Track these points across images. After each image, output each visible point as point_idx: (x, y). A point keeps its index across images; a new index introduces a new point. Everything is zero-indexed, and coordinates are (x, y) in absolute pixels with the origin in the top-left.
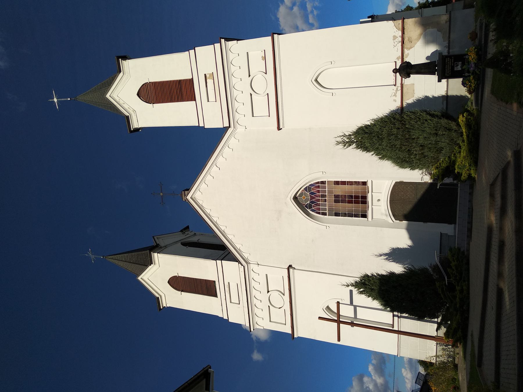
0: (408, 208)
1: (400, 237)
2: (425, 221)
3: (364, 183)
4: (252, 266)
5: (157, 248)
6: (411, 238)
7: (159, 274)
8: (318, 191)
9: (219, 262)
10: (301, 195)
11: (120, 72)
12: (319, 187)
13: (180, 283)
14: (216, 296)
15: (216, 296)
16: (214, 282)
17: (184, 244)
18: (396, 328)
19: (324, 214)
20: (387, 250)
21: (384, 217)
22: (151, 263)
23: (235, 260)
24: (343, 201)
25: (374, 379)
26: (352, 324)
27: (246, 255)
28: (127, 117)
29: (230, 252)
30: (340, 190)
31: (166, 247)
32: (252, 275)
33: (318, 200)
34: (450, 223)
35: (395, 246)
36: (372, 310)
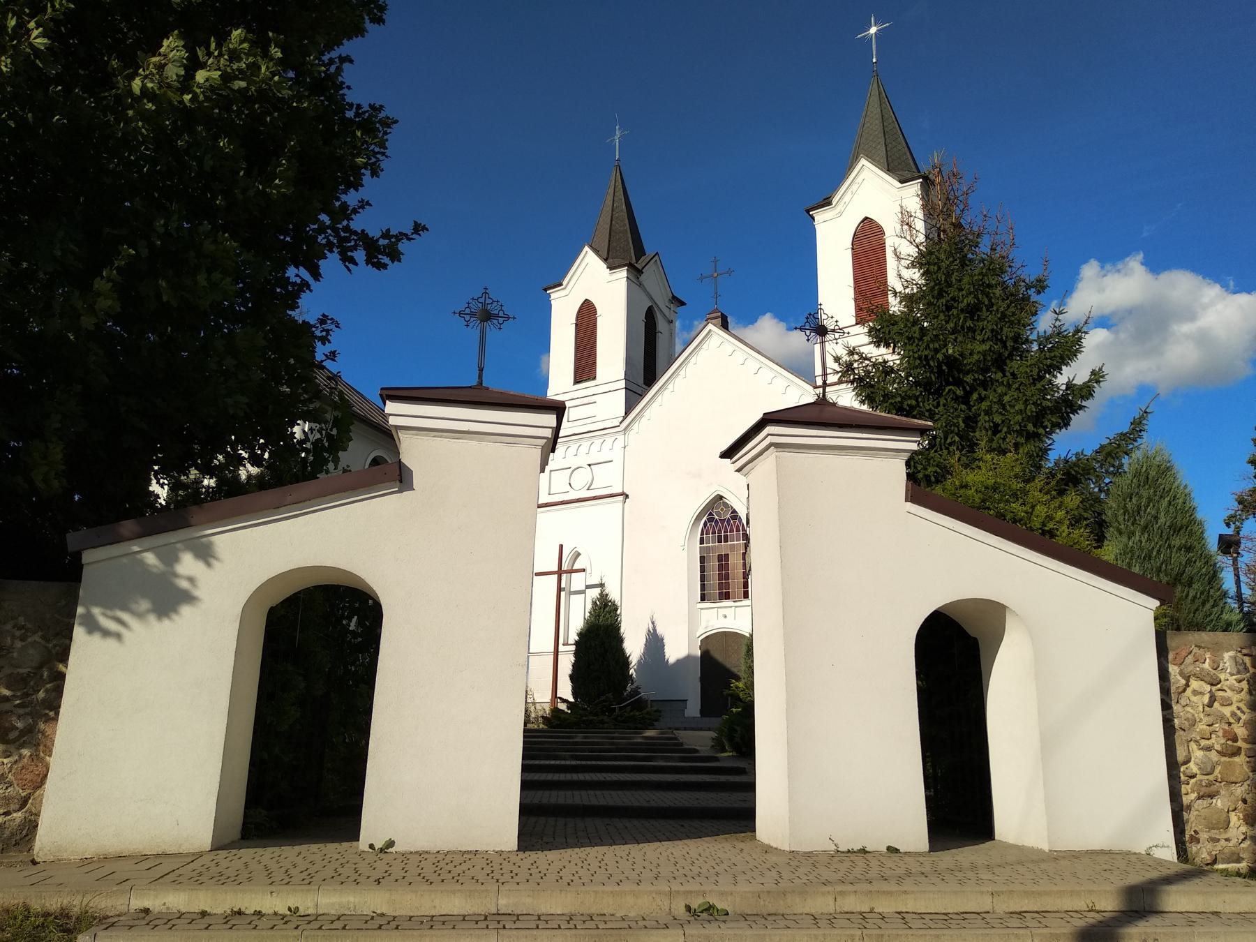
0: (718, 655)
1: (678, 648)
2: (702, 679)
3: (746, 595)
4: (621, 438)
5: (636, 273)
6: (678, 661)
7: (595, 283)
8: (732, 531)
9: (623, 384)
10: (726, 505)
11: (902, 182)
12: (738, 530)
13: (587, 316)
14: (577, 382)
15: (577, 382)
16: (594, 378)
17: (650, 316)
18: (561, 648)
19: (702, 542)
20: (660, 631)
21: (704, 624)
22: (611, 268)
23: (627, 413)
24: (720, 568)
25: (26, 652)
26: (560, 590)
27: (635, 427)
28: (830, 203)
29: (642, 396)
30: (735, 560)
31: (640, 285)
32: (609, 440)
33: (720, 531)
34: (702, 712)
35: (665, 641)
36: (577, 617)
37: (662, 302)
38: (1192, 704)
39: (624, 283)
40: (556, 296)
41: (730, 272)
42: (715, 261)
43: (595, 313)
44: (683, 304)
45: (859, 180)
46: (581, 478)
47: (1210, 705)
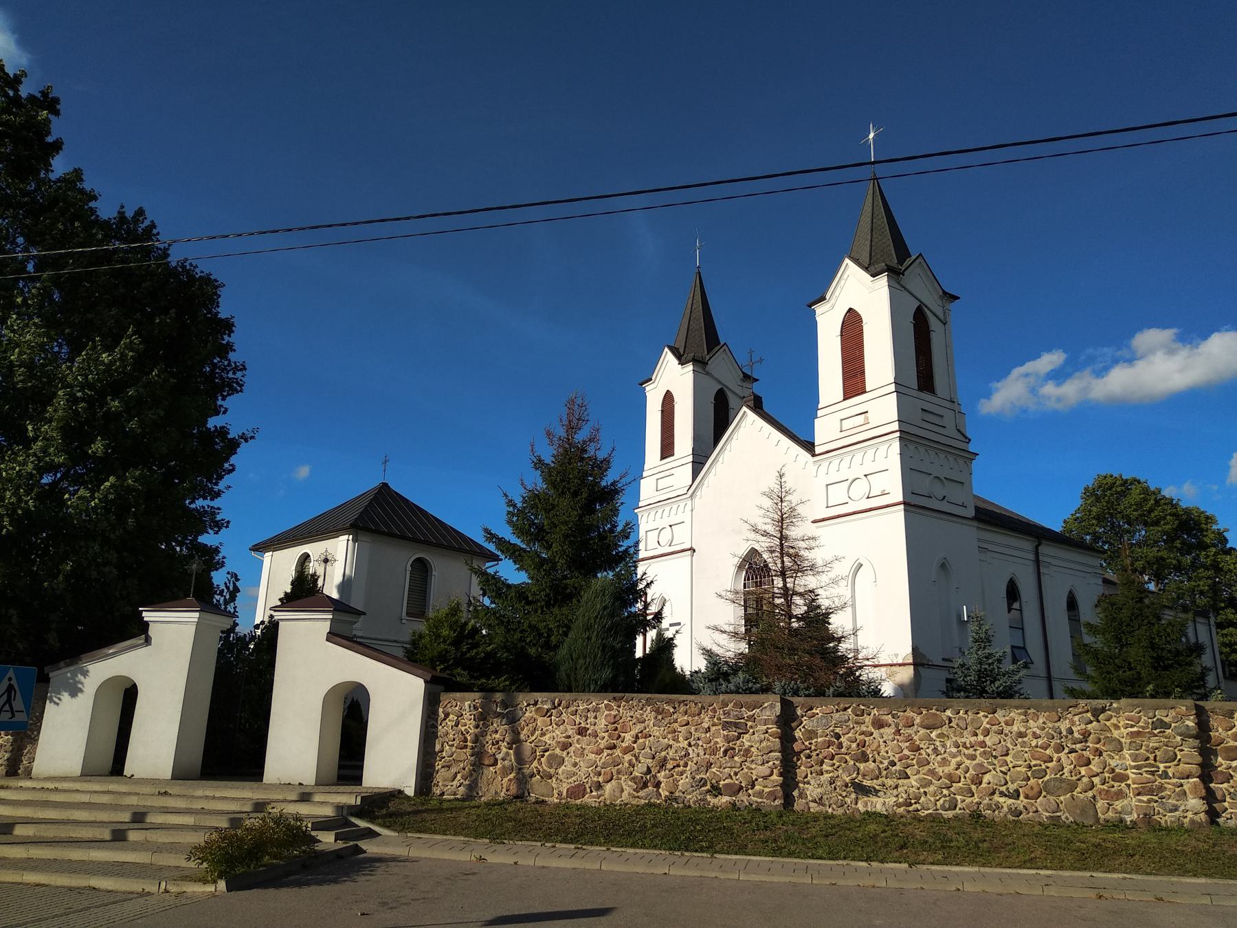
5: (895, 274)
13: (852, 325)
14: (662, 458)
15: (662, 458)
23: (694, 480)
28: (824, 299)
29: (703, 464)
37: (932, 301)
38: (445, 727)
39: (691, 375)
40: (649, 388)
41: (761, 361)
42: (751, 352)
43: (861, 320)
44: (957, 298)
45: (845, 277)
46: (860, 489)
47: (457, 725)
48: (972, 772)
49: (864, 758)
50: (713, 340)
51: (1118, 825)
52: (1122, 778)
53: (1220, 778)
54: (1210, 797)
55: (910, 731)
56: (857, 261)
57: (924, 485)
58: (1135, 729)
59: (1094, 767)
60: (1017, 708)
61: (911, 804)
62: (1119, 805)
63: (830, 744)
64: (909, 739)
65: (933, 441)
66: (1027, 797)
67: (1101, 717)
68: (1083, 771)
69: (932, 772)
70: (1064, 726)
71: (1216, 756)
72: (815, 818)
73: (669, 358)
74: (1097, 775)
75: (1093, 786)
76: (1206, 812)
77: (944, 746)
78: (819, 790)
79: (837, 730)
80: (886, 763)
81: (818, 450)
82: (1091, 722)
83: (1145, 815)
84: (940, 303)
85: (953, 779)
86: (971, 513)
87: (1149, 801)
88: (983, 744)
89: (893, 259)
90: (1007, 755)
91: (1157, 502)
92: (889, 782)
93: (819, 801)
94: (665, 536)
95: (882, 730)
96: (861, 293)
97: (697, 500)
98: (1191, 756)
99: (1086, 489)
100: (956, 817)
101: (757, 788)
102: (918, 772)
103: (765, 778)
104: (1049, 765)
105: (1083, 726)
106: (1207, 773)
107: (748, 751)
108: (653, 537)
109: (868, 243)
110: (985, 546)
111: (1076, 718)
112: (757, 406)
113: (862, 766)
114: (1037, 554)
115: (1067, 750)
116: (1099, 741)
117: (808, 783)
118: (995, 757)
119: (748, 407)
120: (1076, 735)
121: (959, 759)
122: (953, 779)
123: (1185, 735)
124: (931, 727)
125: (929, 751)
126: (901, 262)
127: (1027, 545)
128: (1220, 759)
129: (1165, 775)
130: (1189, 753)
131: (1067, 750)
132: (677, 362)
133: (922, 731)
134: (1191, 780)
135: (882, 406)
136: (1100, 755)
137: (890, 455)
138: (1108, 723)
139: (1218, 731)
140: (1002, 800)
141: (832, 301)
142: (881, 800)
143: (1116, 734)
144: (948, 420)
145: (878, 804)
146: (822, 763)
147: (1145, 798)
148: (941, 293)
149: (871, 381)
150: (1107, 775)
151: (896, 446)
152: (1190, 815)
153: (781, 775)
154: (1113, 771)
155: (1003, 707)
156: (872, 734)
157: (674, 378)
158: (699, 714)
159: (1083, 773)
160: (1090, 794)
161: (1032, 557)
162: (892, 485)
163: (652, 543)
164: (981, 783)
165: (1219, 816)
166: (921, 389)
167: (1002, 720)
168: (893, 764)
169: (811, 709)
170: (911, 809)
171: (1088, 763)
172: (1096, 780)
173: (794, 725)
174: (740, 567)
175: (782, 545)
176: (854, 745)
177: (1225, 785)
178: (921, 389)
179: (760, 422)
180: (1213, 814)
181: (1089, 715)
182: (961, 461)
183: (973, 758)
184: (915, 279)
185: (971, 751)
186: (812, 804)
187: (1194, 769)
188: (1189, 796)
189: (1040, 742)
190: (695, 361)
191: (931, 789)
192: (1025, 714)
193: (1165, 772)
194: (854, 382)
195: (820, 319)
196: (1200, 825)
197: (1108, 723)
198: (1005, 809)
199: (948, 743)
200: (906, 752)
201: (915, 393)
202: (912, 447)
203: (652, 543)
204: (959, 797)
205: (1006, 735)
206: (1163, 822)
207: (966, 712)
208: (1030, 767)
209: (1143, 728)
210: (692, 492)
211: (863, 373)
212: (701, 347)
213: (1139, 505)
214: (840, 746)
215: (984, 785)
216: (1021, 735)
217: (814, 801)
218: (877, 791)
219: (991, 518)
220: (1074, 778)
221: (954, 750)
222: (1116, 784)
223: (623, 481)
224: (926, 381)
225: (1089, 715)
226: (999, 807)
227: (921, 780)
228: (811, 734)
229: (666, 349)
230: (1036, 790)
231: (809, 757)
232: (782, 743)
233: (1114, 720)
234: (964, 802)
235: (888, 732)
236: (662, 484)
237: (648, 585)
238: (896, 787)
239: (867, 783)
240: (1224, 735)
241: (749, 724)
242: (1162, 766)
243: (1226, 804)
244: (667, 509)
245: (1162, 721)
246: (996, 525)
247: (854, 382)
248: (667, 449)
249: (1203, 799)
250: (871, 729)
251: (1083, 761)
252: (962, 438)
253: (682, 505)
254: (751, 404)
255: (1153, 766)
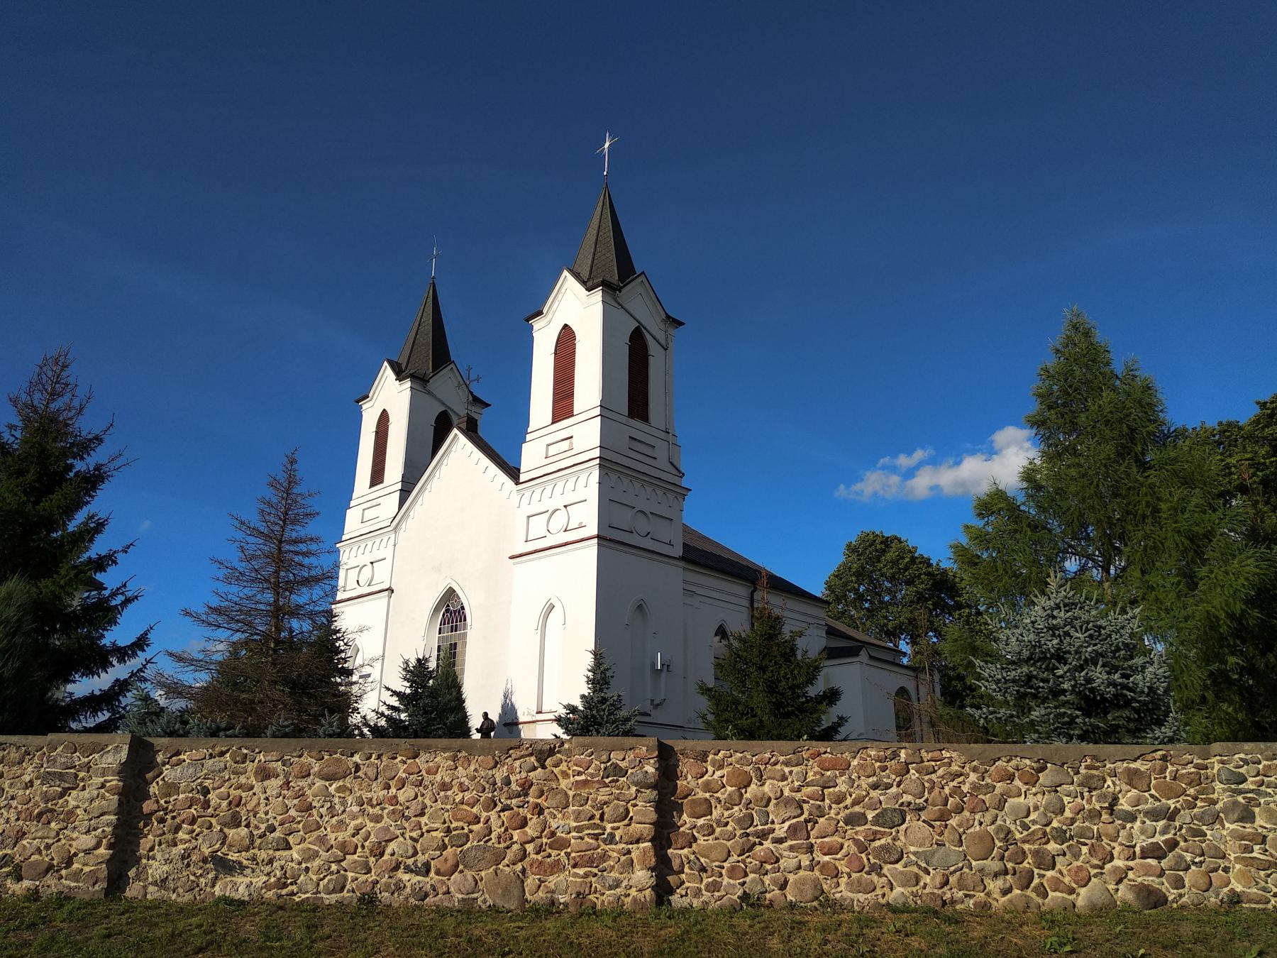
14: (372, 485)
15: (372, 485)
23: (400, 508)
29: (410, 492)
37: (653, 325)
39: (408, 392)
44: (681, 324)
48: (373, 838)
49: (235, 822)
50: (441, 357)
51: (551, 908)
52: (562, 844)
53: (681, 841)
54: (662, 868)
55: (302, 783)
56: (577, 276)
57: (625, 518)
58: (583, 777)
59: (530, 831)
60: (444, 750)
61: (285, 886)
62: (552, 881)
63: (192, 803)
64: (300, 795)
65: (635, 473)
66: (438, 873)
67: (548, 762)
68: (516, 835)
69: (322, 840)
70: (499, 774)
71: (681, 813)
72: (156, 905)
73: (387, 373)
74: (532, 840)
75: (524, 855)
76: (653, 888)
77: (343, 802)
78: (166, 868)
79: (207, 783)
80: (263, 827)
81: (523, 478)
82: (535, 769)
83: (578, 894)
84: (663, 327)
85: (346, 849)
86: (678, 551)
87: (586, 875)
88: (394, 800)
89: (615, 278)
90: (422, 814)
91: (913, 560)
92: (263, 855)
93: (162, 883)
94: (366, 573)
95: (266, 783)
96: (576, 308)
97: (401, 533)
98: (644, 814)
99: (849, 546)
100: (340, 903)
101: (76, 866)
102: (303, 840)
103: (87, 852)
104: (474, 827)
105: (524, 775)
106: (663, 833)
107: (71, 813)
108: (353, 574)
109: (590, 257)
110: (693, 588)
111: (517, 763)
112: (471, 431)
113: (231, 833)
114: (752, 600)
115: (498, 808)
116: (541, 793)
117: (154, 858)
118: (408, 819)
119: (460, 429)
120: (514, 786)
121: (359, 821)
122: (346, 849)
123: (641, 786)
124: (330, 778)
125: (323, 811)
126: (621, 279)
127: (740, 590)
128: (685, 816)
129: (611, 839)
130: (643, 810)
131: (498, 808)
132: (394, 377)
133: (319, 783)
134: (642, 845)
135: (586, 433)
136: (541, 812)
137: (588, 486)
138: (556, 770)
139: (687, 780)
140: (406, 877)
141: (550, 316)
142: (248, 880)
143: (564, 784)
144: (661, 451)
145: (240, 887)
146: (178, 828)
147: (581, 871)
148: (664, 316)
149: (578, 406)
150: (545, 840)
151: (596, 473)
152: (633, 892)
153: (110, 846)
154: (553, 834)
155: (427, 749)
156: (252, 788)
157: (391, 396)
158: (21, 762)
159: (515, 838)
160: (519, 867)
161: (746, 603)
162: (588, 518)
163: (351, 583)
164: (382, 854)
165: (671, 891)
166: (632, 414)
167: (423, 767)
168: (272, 829)
169: (178, 753)
170: (284, 892)
171: (524, 823)
172: (530, 848)
173: (149, 776)
174: (437, 610)
175: (280, 549)
176: (225, 803)
177: (686, 851)
178: (632, 414)
179: (470, 446)
180: (663, 890)
181: (533, 759)
182: (671, 496)
183: (378, 819)
184: (635, 296)
185: (377, 810)
186: (151, 889)
187: (647, 830)
188: (637, 867)
189: (467, 795)
190: (413, 377)
191: (317, 862)
192: (455, 759)
193: (612, 836)
194: (563, 406)
195: (537, 335)
196: (643, 906)
197: (556, 770)
198: (408, 890)
199: (350, 799)
200: (293, 813)
201: (624, 419)
202: (613, 476)
203: (351, 583)
204: (350, 875)
205: (426, 787)
206: (599, 903)
207: (379, 757)
208: (448, 830)
209: (592, 775)
210: (396, 524)
211: (572, 395)
212: (427, 363)
213: (895, 563)
214: (206, 805)
215: (386, 857)
216: (445, 787)
217: (155, 883)
218: (242, 868)
219: (704, 558)
220: (502, 845)
221: (355, 809)
222: (554, 853)
223: (112, 466)
224: (638, 405)
225: (533, 759)
226: (400, 887)
227: (304, 851)
228: (172, 788)
229: (386, 363)
230: (450, 862)
231: (162, 821)
232: (120, 803)
233: (563, 767)
234: (356, 881)
235: (274, 784)
236: (369, 514)
237: (128, 601)
238: (271, 862)
239: (233, 856)
240: (693, 784)
241: (81, 774)
242: (609, 827)
243: (683, 876)
244: (370, 543)
245: (616, 766)
246: (706, 566)
247: (563, 406)
248: (377, 476)
249: (652, 869)
250: (253, 781)
251: (518, 821)
252: (675, 472)
253: (385, 539)
254: (464, 426)
255: (597, 827)
